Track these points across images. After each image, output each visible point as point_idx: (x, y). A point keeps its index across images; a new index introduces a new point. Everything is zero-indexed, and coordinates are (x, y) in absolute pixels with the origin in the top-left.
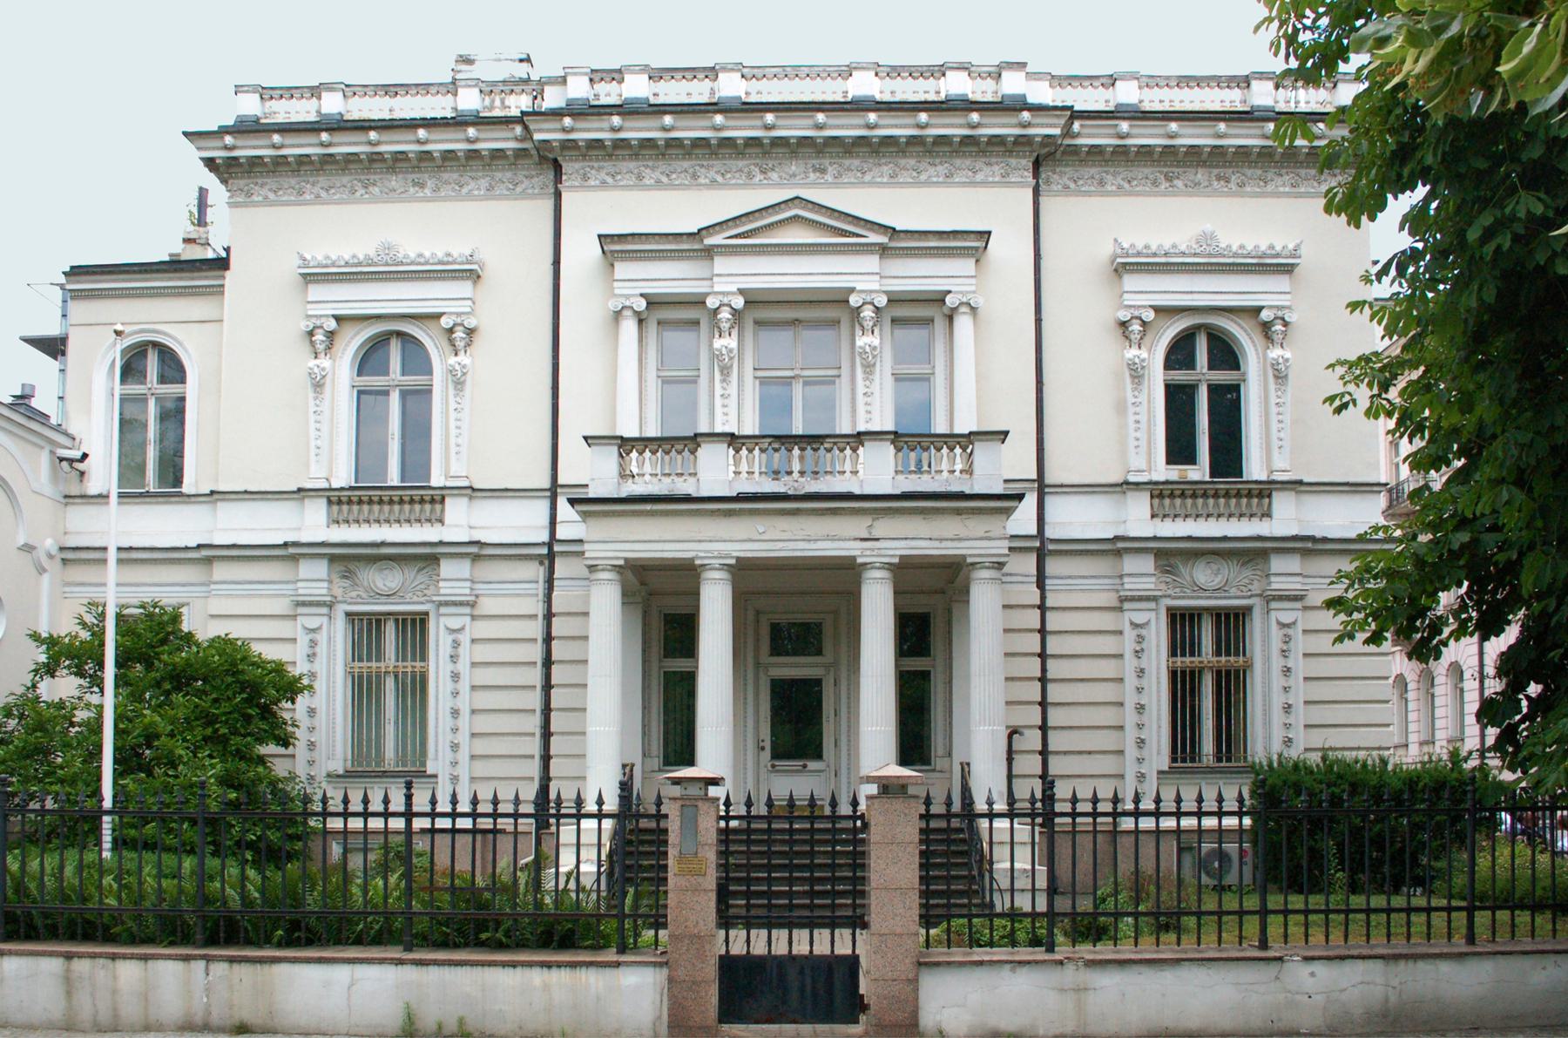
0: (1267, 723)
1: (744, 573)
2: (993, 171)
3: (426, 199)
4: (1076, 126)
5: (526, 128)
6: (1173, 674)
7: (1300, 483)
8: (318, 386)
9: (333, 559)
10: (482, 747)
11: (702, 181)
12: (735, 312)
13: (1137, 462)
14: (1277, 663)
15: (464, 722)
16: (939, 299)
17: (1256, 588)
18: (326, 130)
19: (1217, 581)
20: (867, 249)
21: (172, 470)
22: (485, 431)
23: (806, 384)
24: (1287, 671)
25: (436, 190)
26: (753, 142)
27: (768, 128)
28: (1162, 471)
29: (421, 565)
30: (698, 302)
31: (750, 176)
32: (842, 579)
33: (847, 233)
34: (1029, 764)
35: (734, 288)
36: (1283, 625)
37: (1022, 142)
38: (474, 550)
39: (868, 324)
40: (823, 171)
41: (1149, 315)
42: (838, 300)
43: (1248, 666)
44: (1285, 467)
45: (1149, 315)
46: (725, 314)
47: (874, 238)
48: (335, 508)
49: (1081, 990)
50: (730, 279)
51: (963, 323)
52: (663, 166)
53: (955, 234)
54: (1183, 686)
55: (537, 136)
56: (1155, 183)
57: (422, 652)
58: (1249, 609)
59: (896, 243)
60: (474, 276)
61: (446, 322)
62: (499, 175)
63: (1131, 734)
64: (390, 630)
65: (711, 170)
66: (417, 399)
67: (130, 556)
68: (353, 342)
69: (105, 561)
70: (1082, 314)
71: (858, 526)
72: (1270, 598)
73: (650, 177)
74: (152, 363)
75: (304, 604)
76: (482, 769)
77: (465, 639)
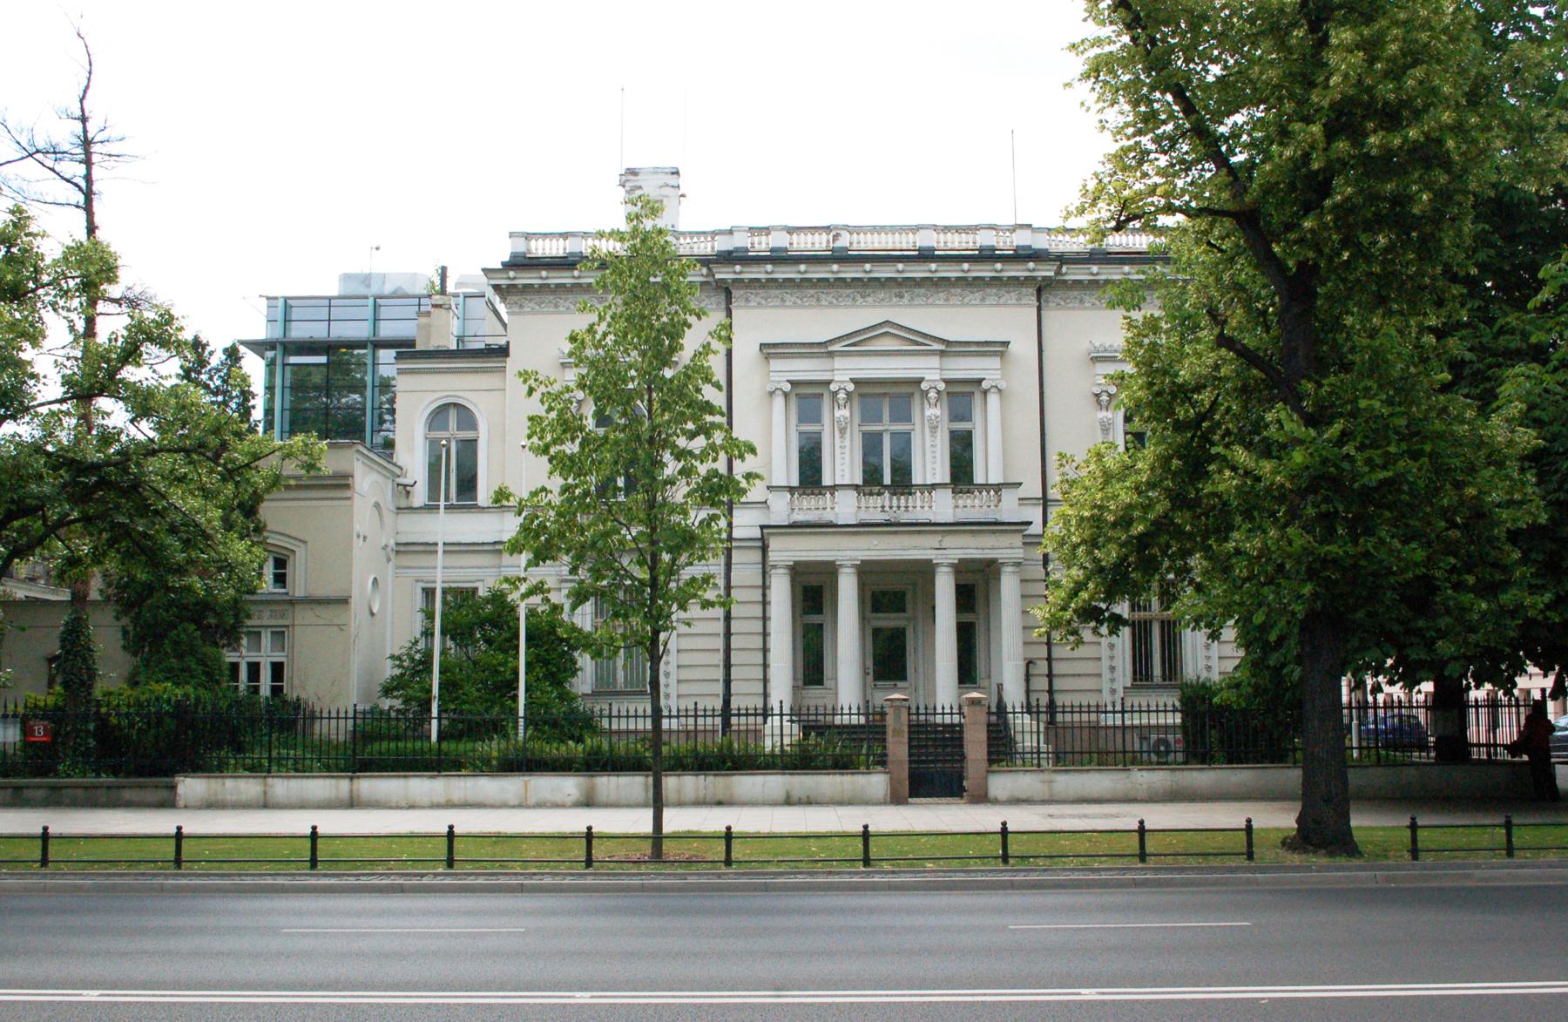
0: (1195, 659)
1: (867, 571)
2: (1012, 297)
4: (1064, 269)
10: (685, 674)
12: (848, 394)
20: (933, 353)
21: (468, 485)
32: (924, 572)
34: (1041, 683)
39: (933, 401)
40: (901, 297)
46: (842, 395)
49: (1051, 782)
50: (844, 372)
51: (993, 399)
53: (987, 343)
59: (949, 349)
63: (1105, 663)
67: (455, 549)
71: (934, 541)
74: (453, 415)
76: (685, 689)
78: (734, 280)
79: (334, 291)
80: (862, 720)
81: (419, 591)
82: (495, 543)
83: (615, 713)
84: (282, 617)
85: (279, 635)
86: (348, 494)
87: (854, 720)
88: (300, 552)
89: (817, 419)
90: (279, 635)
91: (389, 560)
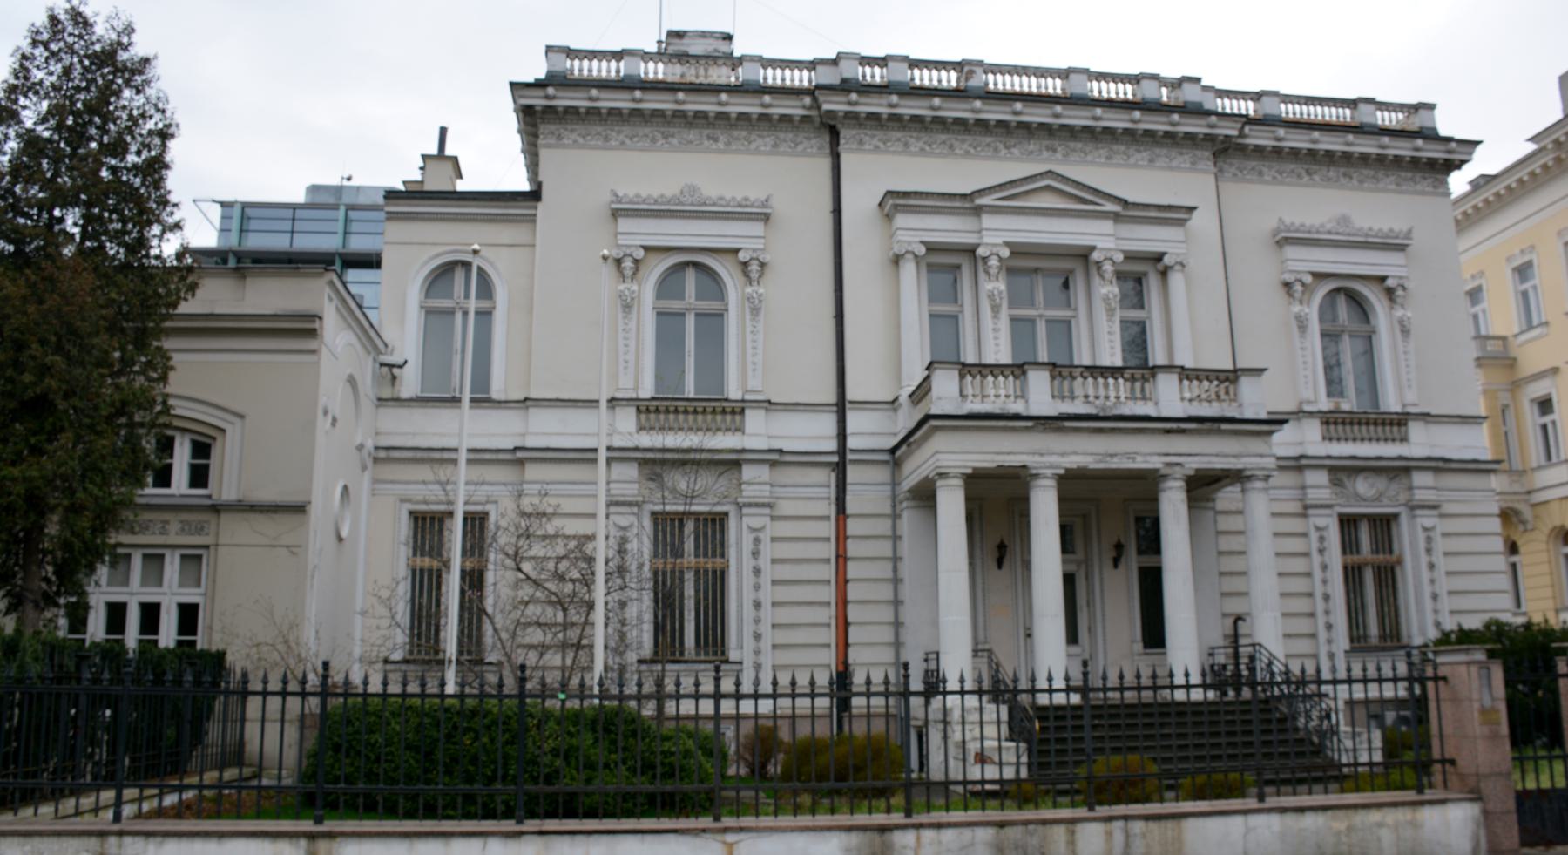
1: (1073, 485)
2: (1183, 159)
3: (719, 151)
5: (815, 99)
6: (1345, 568)
7: (1428, 415)
8: (627, 307)
9: (642, 463)
10: (783, 637)
11: (867, 147)
13: (1307, 394)
14: (748, 562)
15: (767, 614)
16: (1158, 258)
17: (1403, 497)
18: (641, 89)
19: (1371, 493)
22: (772, 353)
23: (1048, 321)
24: (1432, 566)
25: (728, 144)
26: (1001, 124)
27: (1016, 113)
28: (1325, 404)
29: (722, 469)
30: (970, 251)
31: (996, 150)
33: (1087, 201)
35: (1000, 241)
36: (1426, 529)
37: (1210, 138)
38: (775, 457)
41: (1308, 279)
42: (1083, 255)
43: (1400, 562)
44: (1414, 400)
45: (640, 254)
47: (1110, 207)
48: (643, 416)
50: (997, 233)
51: (1176, 280)
52: (925, 137)
54: (1352, 575)
55: (826, 107)
56: (1299, 176)
57: (720, 549)
58: (1396, 516)
59: (1127, 212)
60: (766, 218)
61: (742, 256)
62: (782, 135)
64: (689, 527)
65: (963, 144)
66: (713, 322)
68: (657, 268)
69: (595, 461)
70: (1259, 274)
72: (1413, 507)
73: (915, 145)
75: (617, 504)
76: (785, 657)
77: (765, 537)
78: (847, 114)
79: (299, 197)
80: (1075, 699)
81: (405, 516)
82: (516, 449)
83: (670, 687)
84: (200, 530)
85: (192, 561)
86: (310, 344)
87: (1197, 695)
88: (234, 431)
89: (955, 299)
90: (192, 561)
91: (364, 468)
